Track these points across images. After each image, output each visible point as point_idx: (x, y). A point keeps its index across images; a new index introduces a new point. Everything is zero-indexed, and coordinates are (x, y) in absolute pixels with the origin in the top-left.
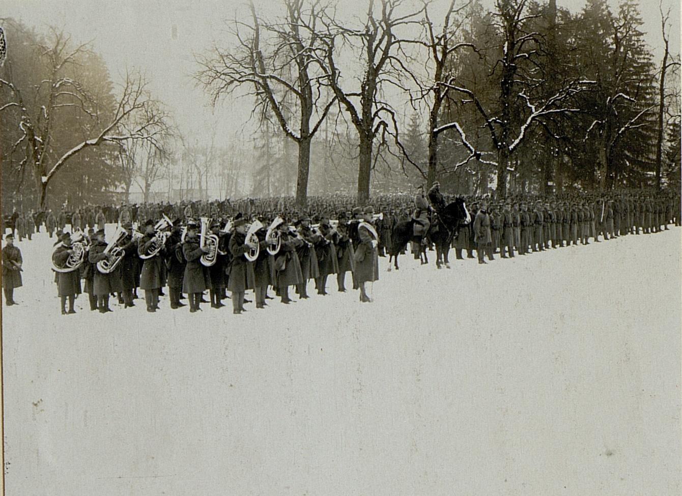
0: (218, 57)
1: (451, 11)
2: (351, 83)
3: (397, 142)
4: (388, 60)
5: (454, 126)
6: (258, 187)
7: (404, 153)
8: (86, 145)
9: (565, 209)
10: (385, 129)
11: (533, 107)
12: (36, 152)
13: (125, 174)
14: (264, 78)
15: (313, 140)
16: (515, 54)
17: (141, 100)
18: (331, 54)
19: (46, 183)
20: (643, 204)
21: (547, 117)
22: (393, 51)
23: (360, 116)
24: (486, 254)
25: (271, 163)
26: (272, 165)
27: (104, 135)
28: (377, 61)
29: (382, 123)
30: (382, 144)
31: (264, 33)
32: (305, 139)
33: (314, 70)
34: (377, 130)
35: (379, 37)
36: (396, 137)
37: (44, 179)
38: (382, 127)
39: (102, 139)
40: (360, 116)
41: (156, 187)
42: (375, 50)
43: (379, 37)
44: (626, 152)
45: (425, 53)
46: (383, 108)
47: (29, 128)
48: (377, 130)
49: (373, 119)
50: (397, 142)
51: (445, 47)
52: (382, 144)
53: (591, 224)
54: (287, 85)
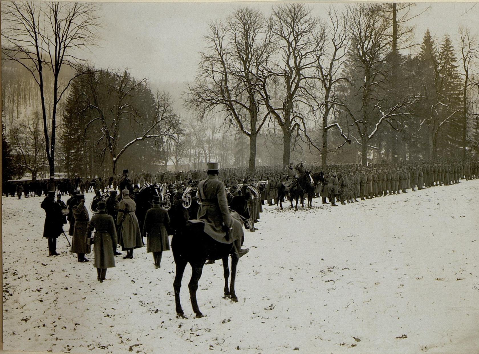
0: (203, 91)
1: (334, 59)
2: (277, 103)
3: (306, 135)
4: (299, 89)
5: (336, 125)
6: (237, 162)
7: (310, 141)
8: (137, 140)
9: (392, 173)
10: (298, 128)
11: (383, 113)
12: (110, 145)
13: (164, 156)
14: (230, 102)
15: (258, 135)
16: (370, 82)
17: (165, 115)
18: (264, 87)
19: (116, 161)
20: (444, 169)
21: (392, 118)
22: (302, 83)
23: (283, 121)
24: (69, 209)
25: (244, 147)
26: (245, 148)
27: (146, 134)
28: (293, 89)
29: (297, 124)
30: (297, 136)
31: (230, 77)
32: (254, 134)
33: (257, 97)
34: (293, 128)
35: (293, 76)
36: (305, 132)
37: (115, 159)
38: (297, 126)
39: (145, 137)
40: (283, 121)
41: (184, 161)
42: (292, 84)
43: (293, 76)
44: (449, 136)
45: (319, 84)
46: (296, 116)
47: (106, 131)
48: (293, 128)
49: (291, 123)
50: (306, 135)
51: (331, 80)
52: (297, 136)
53: (408, 181)
54: (241, 104)
